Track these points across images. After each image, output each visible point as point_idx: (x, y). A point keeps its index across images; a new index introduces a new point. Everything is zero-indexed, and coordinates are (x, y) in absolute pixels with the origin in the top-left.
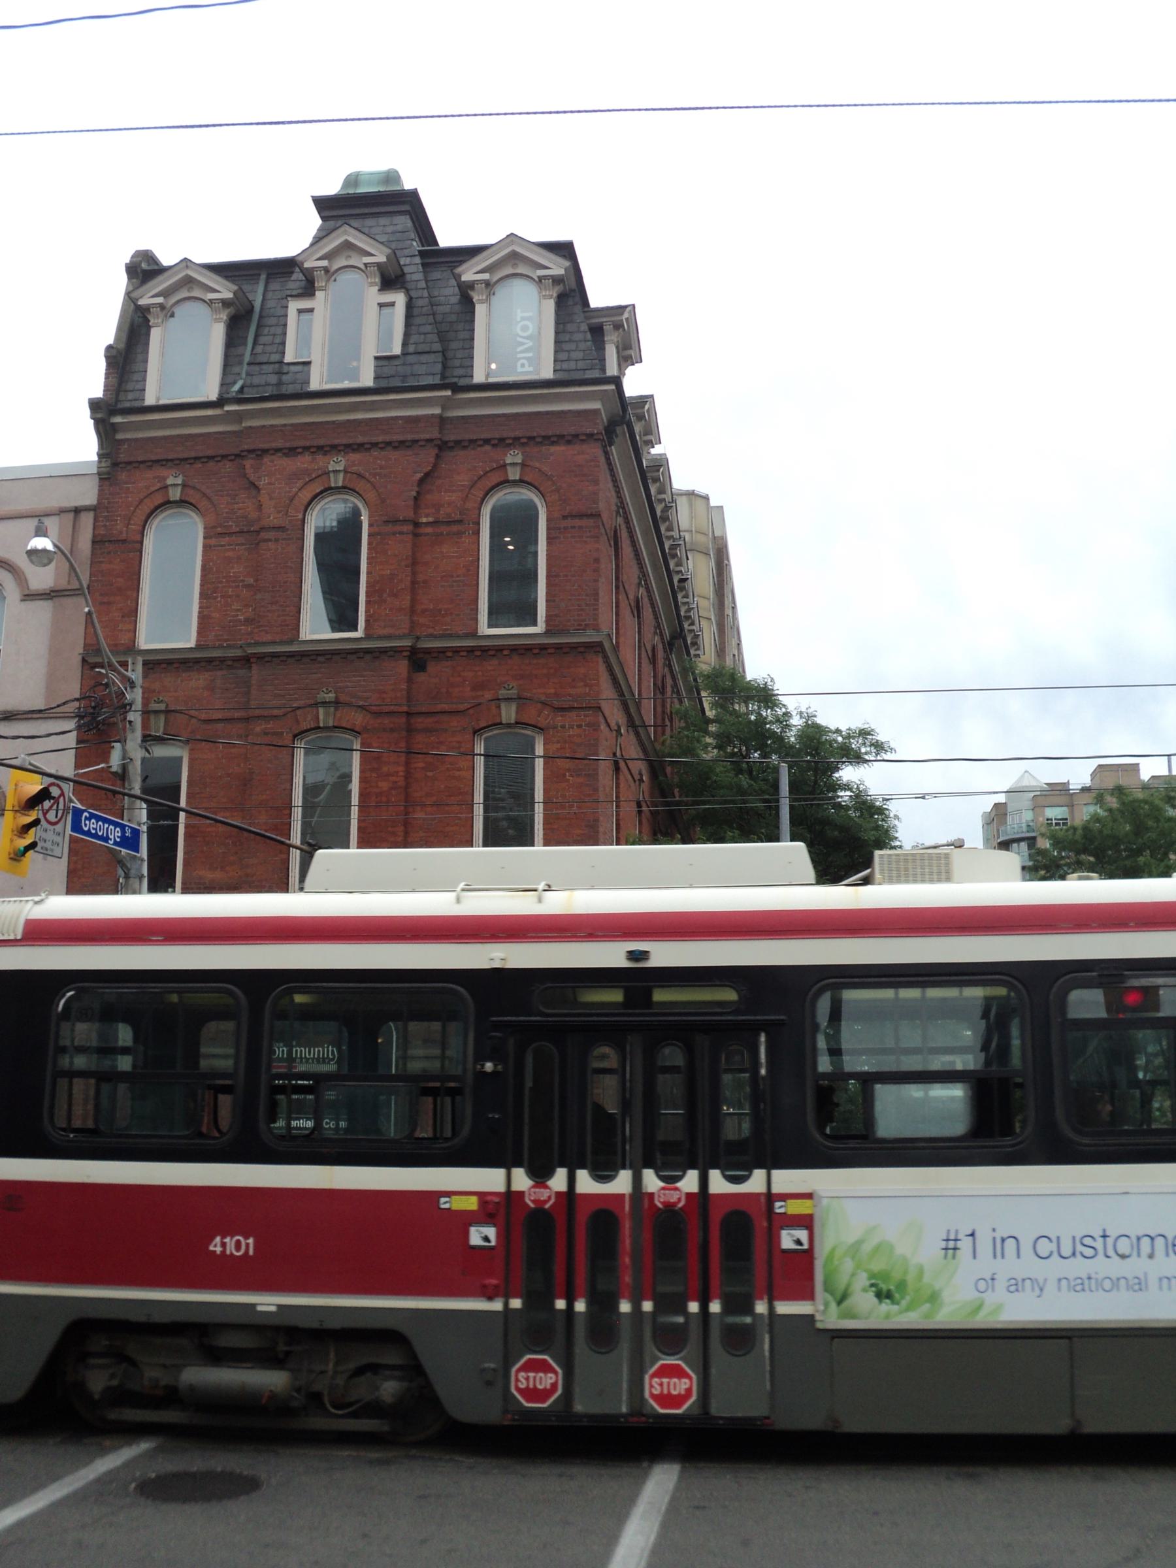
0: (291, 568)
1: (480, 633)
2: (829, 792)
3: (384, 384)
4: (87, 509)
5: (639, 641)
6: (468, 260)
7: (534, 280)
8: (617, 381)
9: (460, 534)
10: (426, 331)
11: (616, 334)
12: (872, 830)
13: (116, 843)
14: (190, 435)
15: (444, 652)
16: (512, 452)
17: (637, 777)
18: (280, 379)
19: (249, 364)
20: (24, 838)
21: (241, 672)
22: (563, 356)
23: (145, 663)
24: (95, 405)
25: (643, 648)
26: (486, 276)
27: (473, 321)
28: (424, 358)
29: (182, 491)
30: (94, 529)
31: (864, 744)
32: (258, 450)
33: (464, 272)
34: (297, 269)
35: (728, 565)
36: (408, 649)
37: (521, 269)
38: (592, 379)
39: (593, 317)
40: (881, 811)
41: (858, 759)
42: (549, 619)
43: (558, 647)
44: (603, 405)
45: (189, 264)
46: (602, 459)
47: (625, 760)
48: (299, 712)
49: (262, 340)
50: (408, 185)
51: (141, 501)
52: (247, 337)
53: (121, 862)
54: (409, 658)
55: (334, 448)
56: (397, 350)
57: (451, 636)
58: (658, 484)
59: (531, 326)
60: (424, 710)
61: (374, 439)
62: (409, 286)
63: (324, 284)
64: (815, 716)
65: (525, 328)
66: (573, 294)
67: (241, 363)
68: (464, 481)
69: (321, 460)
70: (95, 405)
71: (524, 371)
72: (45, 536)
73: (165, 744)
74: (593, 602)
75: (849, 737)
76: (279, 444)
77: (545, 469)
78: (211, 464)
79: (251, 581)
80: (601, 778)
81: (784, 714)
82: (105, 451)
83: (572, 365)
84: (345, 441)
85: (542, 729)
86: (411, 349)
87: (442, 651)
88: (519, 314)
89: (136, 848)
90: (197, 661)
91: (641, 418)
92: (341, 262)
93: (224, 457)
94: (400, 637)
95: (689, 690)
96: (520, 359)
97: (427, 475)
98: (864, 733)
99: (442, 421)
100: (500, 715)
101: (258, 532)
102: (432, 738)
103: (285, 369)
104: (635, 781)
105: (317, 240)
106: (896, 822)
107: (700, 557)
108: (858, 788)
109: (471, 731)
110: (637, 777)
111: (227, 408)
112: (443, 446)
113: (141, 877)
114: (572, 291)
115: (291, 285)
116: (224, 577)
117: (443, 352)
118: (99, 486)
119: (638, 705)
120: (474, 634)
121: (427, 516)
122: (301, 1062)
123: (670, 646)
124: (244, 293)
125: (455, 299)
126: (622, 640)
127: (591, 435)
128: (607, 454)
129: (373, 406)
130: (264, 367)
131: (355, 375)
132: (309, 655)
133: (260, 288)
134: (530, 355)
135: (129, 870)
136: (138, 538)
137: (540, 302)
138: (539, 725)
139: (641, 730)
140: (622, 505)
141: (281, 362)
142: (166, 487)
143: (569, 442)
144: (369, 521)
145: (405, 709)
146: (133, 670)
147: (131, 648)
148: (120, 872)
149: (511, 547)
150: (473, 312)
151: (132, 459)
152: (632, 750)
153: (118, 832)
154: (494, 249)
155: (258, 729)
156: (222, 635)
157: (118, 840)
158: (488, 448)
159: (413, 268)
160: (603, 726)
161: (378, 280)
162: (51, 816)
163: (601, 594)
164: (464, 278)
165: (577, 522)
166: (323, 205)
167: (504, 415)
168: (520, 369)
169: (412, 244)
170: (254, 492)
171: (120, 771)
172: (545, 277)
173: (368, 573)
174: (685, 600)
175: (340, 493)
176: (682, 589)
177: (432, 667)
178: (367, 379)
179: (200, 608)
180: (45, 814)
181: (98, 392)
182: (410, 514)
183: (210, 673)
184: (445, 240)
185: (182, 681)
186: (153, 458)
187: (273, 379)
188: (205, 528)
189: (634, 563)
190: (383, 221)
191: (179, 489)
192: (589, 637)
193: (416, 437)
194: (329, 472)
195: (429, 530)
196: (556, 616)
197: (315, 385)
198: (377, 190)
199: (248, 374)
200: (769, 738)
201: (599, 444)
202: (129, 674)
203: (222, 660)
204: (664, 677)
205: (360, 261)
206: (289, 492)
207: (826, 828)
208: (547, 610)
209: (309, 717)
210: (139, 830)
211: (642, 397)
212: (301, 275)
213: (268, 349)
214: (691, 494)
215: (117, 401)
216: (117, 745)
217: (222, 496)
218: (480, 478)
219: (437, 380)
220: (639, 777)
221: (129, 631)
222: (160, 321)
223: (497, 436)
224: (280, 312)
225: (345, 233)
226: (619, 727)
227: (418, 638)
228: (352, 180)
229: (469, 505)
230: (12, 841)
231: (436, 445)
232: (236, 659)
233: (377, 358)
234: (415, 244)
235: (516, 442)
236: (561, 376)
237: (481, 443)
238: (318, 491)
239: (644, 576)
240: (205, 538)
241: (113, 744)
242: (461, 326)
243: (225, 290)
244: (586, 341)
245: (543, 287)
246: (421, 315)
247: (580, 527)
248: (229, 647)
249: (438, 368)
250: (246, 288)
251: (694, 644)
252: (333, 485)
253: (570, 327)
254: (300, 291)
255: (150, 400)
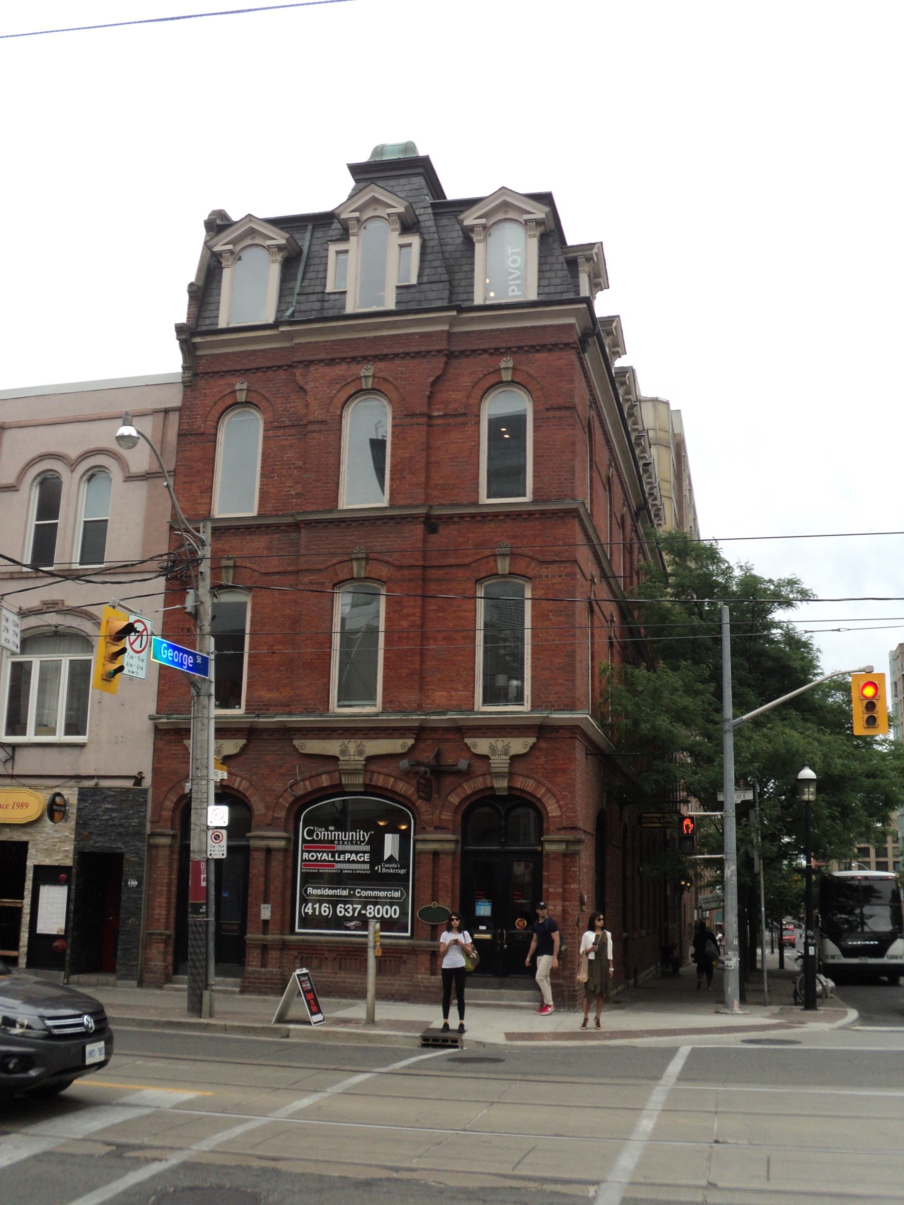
0: (331, 453)
1: (481, 503)
2: (764, 630)
3: (403, 307)
4: (174, 410)
5: (610, 511)
6: (466, 210)
7: (521, 222)
8: (589, 302)
9: (464, 424)
10: (436, 265)
11: (588, 265)
12: (798, 660)
13: (189, 668)
14: (254, 351)
15: (452, 518)
16: (505, 359)
17: (609, 618)
18: (323, 306)
19: (298, 294)
20: (114, 663)
21: (294, 535)
22: (545, 282)
23: (214, 530)
24: (180, 329)
25: (614, 516)
26: (483, 221)
27: (473, 257)
28: (435, 287)
29: (247, 395)
30: (180, 424)
31: (792, 591)
32: (306, 361)
33: (466, 218)
34: (336, 221)
35: (685, 456)
36: (424, 515)
37: (511, 215)
38: (567, 300)
39: (570, 252)
40: (806, 645)
41: (788, 603)
42: (535, 491)
43: (543, 513)
44: (577, 321)
45: (252, 218)
46: (577, 364)
47: (596, 601)
48: (337, 566)
49: (309, 275)
50: (422, 153)
51: (215, 403)
52: (296, 274)
53: (193, 684)
54: (425, 523)
55: (365, 359)
56: (414, 280)
57: (457, 505)
58: (625, 387)
59: (519, 261)
60: (436, 564)
61: (397, 351)
62: (424, 231)
63: (356, 231)
64: (752, 569)
65: (514, 262)
66: (552, 234)
67: (292, 295)
68: (467, 382)
69: (354, 368)
70: (180, 329)
71: (514, 295)
72: (130, 425)
73: (233, 592)
74: (570, 477)
75: (779, 586)
76: (322, 356)
77: (531, 372)
78: (270, 373)
79: (301, 464)
80: (577, 617)
81: (727, 568)
82: (187, 365)
83: (552, 289)
84: (373, 353)
85: (530, 579)
86: (425, 279)
87: (450, 517)
88: (510, 251)
89: (205, 672)
90: (259, 527)
91: (610, 333)
92: (369, 213)
93: (280, 367)
94: (417, 507)
95: (652, 551)
96: (511, 285)
97: (438, 378)
98: (791, 583)
99: (449, 335)
100: (496, 566)
101: (306, 425)
102: (443, 586)
103: (327, 298)
104: (607, 621)
105: (351, 197)
106: (818, 654)
107: (663, 451)
108: (787, 627)
109: (473, 581)
110: (609, 618)
111: (281, 329)
112: (450, 356)
113: (210, 695)
114: (552, 231)
115: (332, 233)
116: (279, 461)
117: (450, 281)
118: (184, 392)
119: (610, 562)
120: (475, 504)
121: (438, 410)
122: (339, 844)
123: (636, 515)
124: (295, 241)
125: (459, 240)
126: (595, 508)
127: (567, 345)
128: (581, 360)
129: (394, 325)
130: (310, 296)
131: (381, 301)
132: (345, 521)
133: (308, 236)
134: (519, 282)
135: (200, 689)
136: (213, 431)
137: (526, 241)
138: (528, 575)
139: (612, 580)
140: (594, 400)
141: (323, 293)
142: (235, 392)
143: (550, 350)
144: (393, 415)
145: (421, 563)
146: (204, 532)
147: (208, 517)
148: (193, 692)
149: (507, 436)
150: (473, 250)
151: (209, 370)
152: (602, 591)
153: (191, 660)
154: (489, 199)
155: (306, 580)
156: (278, 506)
157: (191, 666)
158: (486, 356)
159: (426, 217)
160: (579, 576)
161: (398, 226)
162: (137, 646)
163: (577, 470)
164: (466, 223)
165: (558, 413)
166: (356, 170)
167: (498, 330)
168: (511, 294)
169: (425, 199)
170: (303, 395)
171: (193, 612)
172: (530, 221)
173: (392, 456)
174: (649, 480)
175: (369, 394)
176: (646, 471)
177: (443, 530)
178: (390, 304)
179: (261, 485)
180: (131, 644)
181: (183, 319)
182: (425, 410)
183: (269, 536)
184: (452, 192)
185: (247, 542)
186: (224, 369)
187: (317, 306)
188: (265, 423)
189: (605, 448)
190: (403, 181)
191: (245, 392)
192: (568, 505)
193: (429, 348)
194: (361, 377)
195: (439, 421)
196: (542, 488)
197: (349, 309)
198: (397, 157)
199: (298, 302)
200: (716, 587)
201: (574, 351)
202: (201, 535)
203: (278, 526)
204: (631, 539)
205: (383, 212)
206: (329, 394)
207: (762, 659)
208: (534, 484)
209: (346, 570)
210: (207, 658)
211: (610, 317)
212: (339, 224)
213: (313, 282)
214: (655, 401)
215: (197, 326)
216: (191, 591)
217: (279, 397)
218: (480, 379)
219: (445, 303)
220: (610, 618)
221: (206, 504)
222: (230, 263)
223: (493, 346)
224: (323, 253)
225: (373, 190)
226: (593, 577)
227: (431, 507)
228: (379, 150)
229: (471, 401)
230: (104, 665)
231: (445, 355)
232: (288, 525)
233: (398, 287)
234: (427, 198)
235: (508, 351)
236: (542, 298)
237: (480, 352)
238: (352, 392)
239: (614, 459)
240: (265, 430)
241: (188, 590)
242: (464, 261)
243: (280, 238)
244: (562, 270)
245: (528, 228)
246: (433, 253)
247: (560, 418)
248: (284, 515)
249: (446, 294)
250: (297, 236)
251: (657, 515)
252: (364, 388)
253: (550, 260)
254: (338, 237)
255: (222, 324)
